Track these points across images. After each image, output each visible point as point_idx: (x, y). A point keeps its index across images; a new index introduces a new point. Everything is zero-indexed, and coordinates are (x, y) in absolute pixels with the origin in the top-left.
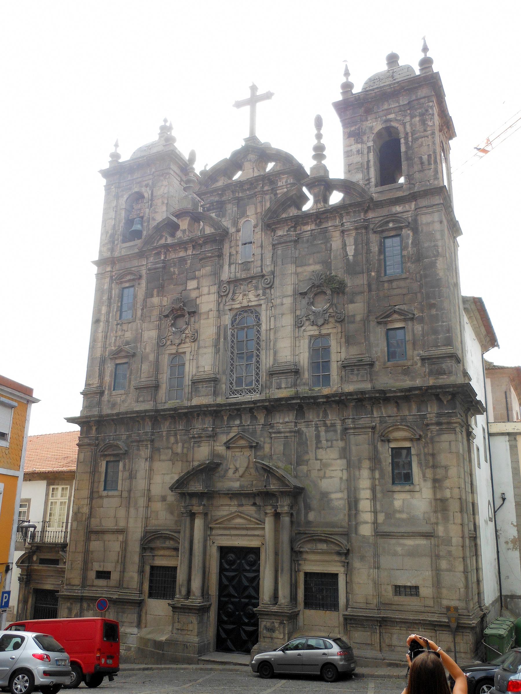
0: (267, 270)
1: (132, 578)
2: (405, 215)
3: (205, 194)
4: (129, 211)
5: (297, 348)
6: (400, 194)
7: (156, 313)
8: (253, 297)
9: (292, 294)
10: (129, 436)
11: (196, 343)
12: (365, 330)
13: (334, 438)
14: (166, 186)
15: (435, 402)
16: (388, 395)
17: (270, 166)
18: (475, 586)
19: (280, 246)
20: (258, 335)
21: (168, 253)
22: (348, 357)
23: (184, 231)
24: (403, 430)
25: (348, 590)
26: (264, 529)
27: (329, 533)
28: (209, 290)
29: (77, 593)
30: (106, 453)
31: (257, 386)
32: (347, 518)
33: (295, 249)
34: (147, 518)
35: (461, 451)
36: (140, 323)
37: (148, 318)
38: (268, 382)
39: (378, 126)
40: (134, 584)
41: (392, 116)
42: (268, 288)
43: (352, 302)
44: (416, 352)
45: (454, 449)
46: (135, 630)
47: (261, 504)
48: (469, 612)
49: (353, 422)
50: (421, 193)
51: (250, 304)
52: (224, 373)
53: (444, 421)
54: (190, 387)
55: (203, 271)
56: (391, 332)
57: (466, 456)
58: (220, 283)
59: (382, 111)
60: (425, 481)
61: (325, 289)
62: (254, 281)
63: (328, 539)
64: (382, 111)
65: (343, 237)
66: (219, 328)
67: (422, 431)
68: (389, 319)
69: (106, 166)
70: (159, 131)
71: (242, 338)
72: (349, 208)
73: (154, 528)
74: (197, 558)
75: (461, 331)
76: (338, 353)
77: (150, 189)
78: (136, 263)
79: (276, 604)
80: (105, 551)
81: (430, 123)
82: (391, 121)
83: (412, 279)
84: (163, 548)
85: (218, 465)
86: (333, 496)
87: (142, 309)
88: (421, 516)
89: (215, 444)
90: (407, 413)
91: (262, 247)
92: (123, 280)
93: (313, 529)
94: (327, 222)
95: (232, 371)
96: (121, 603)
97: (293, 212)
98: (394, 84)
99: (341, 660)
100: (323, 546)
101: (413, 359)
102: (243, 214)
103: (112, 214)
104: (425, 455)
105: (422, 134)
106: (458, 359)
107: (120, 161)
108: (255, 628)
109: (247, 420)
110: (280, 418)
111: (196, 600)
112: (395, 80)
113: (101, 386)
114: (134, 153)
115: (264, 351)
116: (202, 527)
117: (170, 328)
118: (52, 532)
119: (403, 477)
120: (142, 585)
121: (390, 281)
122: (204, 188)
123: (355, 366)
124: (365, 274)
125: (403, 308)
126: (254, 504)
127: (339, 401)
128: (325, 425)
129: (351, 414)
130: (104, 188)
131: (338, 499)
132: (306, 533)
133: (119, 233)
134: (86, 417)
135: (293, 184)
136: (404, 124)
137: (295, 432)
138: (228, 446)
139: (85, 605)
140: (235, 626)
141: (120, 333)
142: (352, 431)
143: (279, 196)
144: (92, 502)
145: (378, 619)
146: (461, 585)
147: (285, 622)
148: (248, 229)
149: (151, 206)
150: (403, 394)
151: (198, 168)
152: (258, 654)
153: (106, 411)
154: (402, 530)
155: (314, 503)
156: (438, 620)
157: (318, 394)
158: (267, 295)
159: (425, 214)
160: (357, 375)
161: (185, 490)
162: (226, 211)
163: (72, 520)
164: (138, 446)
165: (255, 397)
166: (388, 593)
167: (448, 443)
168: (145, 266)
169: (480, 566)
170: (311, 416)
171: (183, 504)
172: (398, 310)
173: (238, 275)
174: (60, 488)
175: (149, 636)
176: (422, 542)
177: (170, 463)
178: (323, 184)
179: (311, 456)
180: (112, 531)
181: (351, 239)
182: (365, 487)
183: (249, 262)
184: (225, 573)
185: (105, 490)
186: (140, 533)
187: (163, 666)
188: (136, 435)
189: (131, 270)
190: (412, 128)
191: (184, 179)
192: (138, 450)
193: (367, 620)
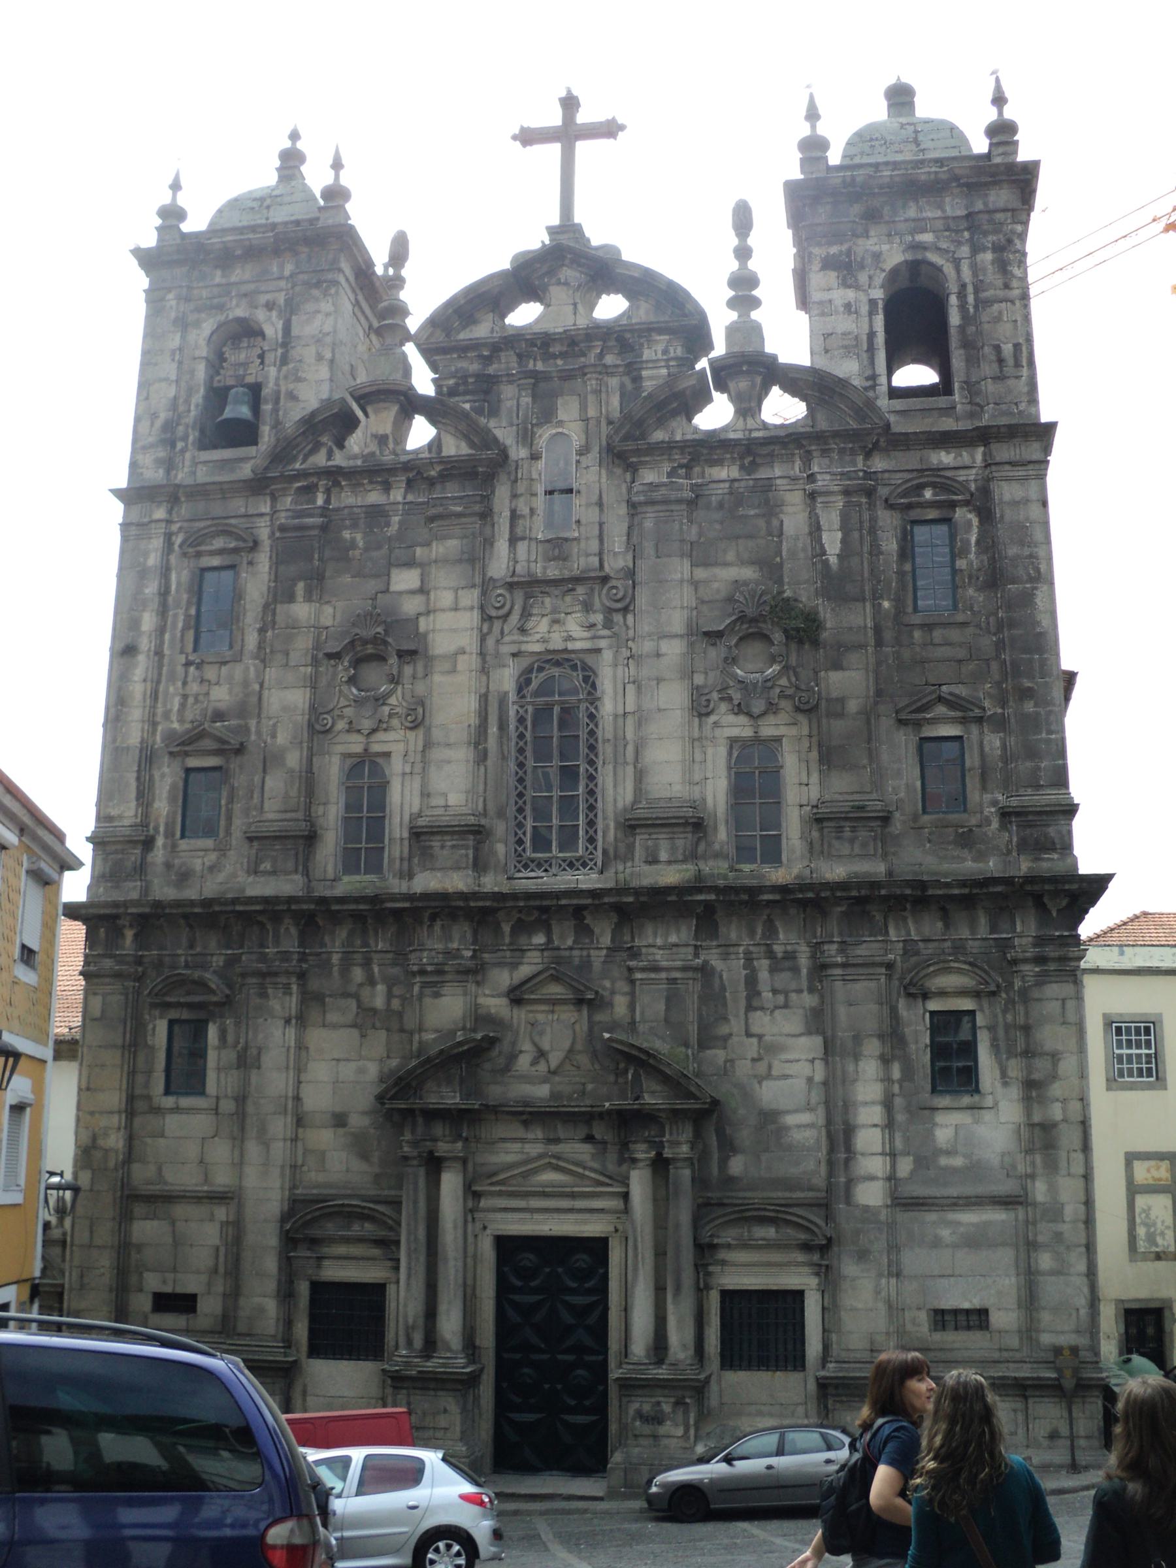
0: (616, 563)
1: (261, 1310)
2: (962, 476)
4: (217, 362)
5: (697, 767)
7: (303, 644)
8: (578, 628)
10: (231, 961)
11: (421, 732)
13: (793, 986)
14: (328, 315)
19: (649, 509)
21: (335, 491)
22: (827, 797)
24: (959, 971)
27: (783, 1202)
28: (456, 598)
30: (168, 999)
31: (591, 853)
32: (823, 1169)
34: (294, 1167)
36: (254, 665)
37: (279, 657)
39: (894, 256)
41: (927, 237)
43: (837, 666)
44: (987, 797)
52: (501, 814)
53: (1052, 955)
54: (406, 843)
55: (438, 549)
58: (486, 586)
59: (906, 220)
60: (1005, 1084)
61: (766, 627)
62: (581, 590)
63: (780, 1215)
66: (484, 698)
71: (552, 728)
73: (315, 1191)
74: (451, 1263)
76: (800, 785)
77: (279, 317)
78: (238, 505)
82: (925, 249)
83: (978, 626)
84: (347, 1240)
85: (491, 1042)
86: (790, 1120)
87: (262, 631)
88: (995, 1161)
90: (965, 933)
92: (203, 548)
93: (741, 1194)
94: (771, 465)
100: (770, 1232)
101: (982, 812)
102: (547, 415)
104: (1007, 1027)
105: (1001, 293)
107: (185, 227)
110: (655, 935)
113: (144, 825)
115: (611, 767)
117: (345, 688)
119: (953, 1068)
121: (928, 627)
124: (868, 604)
125: (957, 692)
126: (589, 1139)
127: (808, 901)
128: (770, 954)
129: (836, 932)
130: (143, 295)
131: (803, 1126)
136: (957, 263)
141: (194, 688)
142: (838, 971)
144: (131, 1124)
146: (1082, 1301)
153: (162, 890)
154: (953, 1191)
155: (744, 1136)
156: (1035, 1375)
159: (1008, 479)
160: (852, 841)
162: (499, 401)
164: (262, 986)
165: (587, 880)
167: (1060, 1002)
170: (732, 931)
173: (538, 570)
176: (997, 1216)
177: (355, 1033)
179: (735, 1025)
181: (834, 514)
183: (566, 540)
188: (254, 957)
192: (264, 995)
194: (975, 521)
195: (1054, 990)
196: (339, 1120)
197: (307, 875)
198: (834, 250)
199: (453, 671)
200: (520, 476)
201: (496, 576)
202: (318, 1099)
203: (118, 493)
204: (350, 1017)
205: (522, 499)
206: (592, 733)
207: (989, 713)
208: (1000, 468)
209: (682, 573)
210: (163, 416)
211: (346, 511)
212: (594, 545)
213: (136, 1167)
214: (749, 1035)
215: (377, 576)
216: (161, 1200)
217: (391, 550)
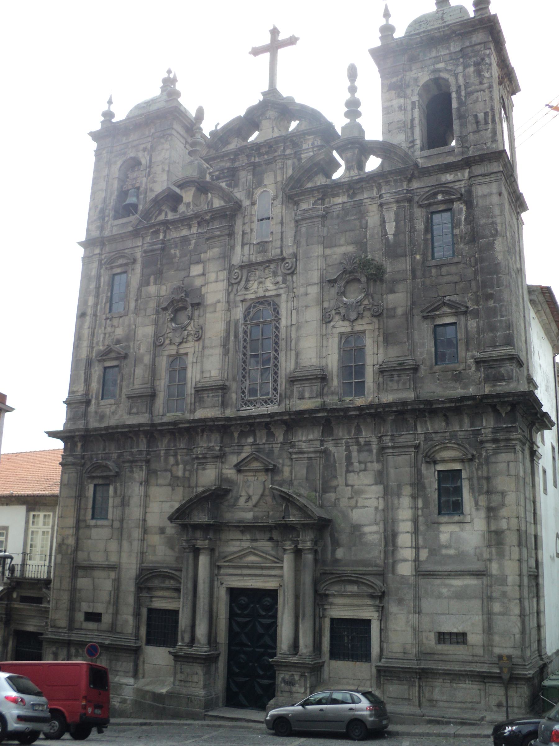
0: (288, 252)
1: (126, 621)
2: (457, 185)
3: (214, 159)
4: (123, 180)
5: (324, 349)
6: (451, 159)
7: (152, 305)
8: (271, 285)
9: (319, 281)
10: (120, 456)
11: (201, 342)
12: (408, 326)
14: (167, 150)
16: (434, 406)
17: (294, 125)
18: (534, 632)
19: (304, 222)
20: (277, 332)
22: (386, 360)
23: (188, 205)
24: (453, 448)
25: (383, 639)
26: (282, 568)
29: (64, 636)
30: (94, 474)
31: (275, 396)
33: (323, 226)
34: (142, 553)
35: (521, 474)
38: (288, 391)
39: (424, 77)
40: (129, 628)
41: (441, 65)
42: (289, 274)
43: (392, 291)
44: (469, 354)
45: (513, 472)
46: (131, 681)
47: (279, 539)
48: (524, 661)
49: (392, 440)
50: (477, 158)
51: (267, 294)
52: (234, 379)
54: (193, 396)
55: (211, 253)
56: (439, 329)
57: (529, 479)
58: (231, 268)
59: (430, 59)
60: (477, 509)
61: (358, 275)
62: (272, 266)
63: (359, 580)
64: (430, 59)
65: (382, 211)
66: (228, 323)
67: (476, 450)
68: (437, 313)
69: (97, 127)
70: (162, 84)
71: (257, 337)
72: (389, 177)
73: (151, 565)
74: (202, 600)
75: (525, 328)
76: (374, 355)
79: (296, 654)
80: (94, 589)
81: (487, 75)
82: (440, 71)
83: (465, 263)
84: (163, 589)
85: (227, 491)
86: (367, 529)
87: (137, 300)
90: (457, 428)
91: (282, 223)
94: (362, 192)
95: (244, 377)
96: (114, 650)
97: (320, 180)
98: (444, 27)
99: (371, 716)
100: (354, 588)
101: (466, 363)
102: (260, 183)
103: (103, 185)
104: (479, 478)
105: (478, 87)
106: (519, 362)
107: (114, 120)
108: (272, 681)
109: (262, 438)
110: (302, 435)
111: (202, 648)
112: (445, 22)
113: (87, 394)
114: (131, 111)
115: (284, 352)
116: (208, 566)
117: (169, 324)
118: (34, 566)
120: (138, 631)
121: (439, 266)
122: (212, 152)
123: (395, 370)
124: (408, 258)
126: (271, 539)
127: (375, 414)
128: (358, 443)
130: (94, 153)
131: (373, 532)
132: (332, 574)
133: (110, 207)
134: (70, 431)
135: (321, 147)
136: (456, 76)
137: (320, 452)
139: (73, 651)
140: (248, 679)
141: (109, 329)
142: (391, 451)
143: (303, 161)
144: (78, 531)
145: (417, 671)
146: (517, 630)
147: (306, 674)
148: (265, 201)
149: (149, 175)
150: (453, 405)
151: (207, 128)
152: (274, 708)
153: (94, 424)
155: (344, 538)
156: (488, 671)
157: (350, 406)
158: (288, 283)
159: (480, 184)
160: (398, 382)
161: (186, 521)
163: (55, 553)
164: (131, 467)
165: (272, 408)
166: (430, 641)
168: (140, 248)
169: (542, 609)
171: (185, 538)
173: (253, 258)
174: (42, 514)
175: (148, 688)
176: (472, 582)
177: (170, 488)
178: (358, 148)
179: (340, 481)
180: (101, 567)
182: (405, 518)
183: (266, 242)
184: (236, 619)
185: (93, 518)
186: (134, 571)
187: (163, 721)
188: (128, 453)
189: (124, 253)
190: (465, 80)
191: (190, 140)
192: (132, 471)
194: (464, 208)
197: (152, 414)
199: (215, 311)
203: (81, 244)
204: (168, 481)
205: (247, 225)
208: (476, 178)
209: (318, 252)
210: (100, 207)
212: (278, 243)
213: (80, 553)
214: (347, 485)
215: (184, 270)
216: (90, 568)
217: (191, 256)
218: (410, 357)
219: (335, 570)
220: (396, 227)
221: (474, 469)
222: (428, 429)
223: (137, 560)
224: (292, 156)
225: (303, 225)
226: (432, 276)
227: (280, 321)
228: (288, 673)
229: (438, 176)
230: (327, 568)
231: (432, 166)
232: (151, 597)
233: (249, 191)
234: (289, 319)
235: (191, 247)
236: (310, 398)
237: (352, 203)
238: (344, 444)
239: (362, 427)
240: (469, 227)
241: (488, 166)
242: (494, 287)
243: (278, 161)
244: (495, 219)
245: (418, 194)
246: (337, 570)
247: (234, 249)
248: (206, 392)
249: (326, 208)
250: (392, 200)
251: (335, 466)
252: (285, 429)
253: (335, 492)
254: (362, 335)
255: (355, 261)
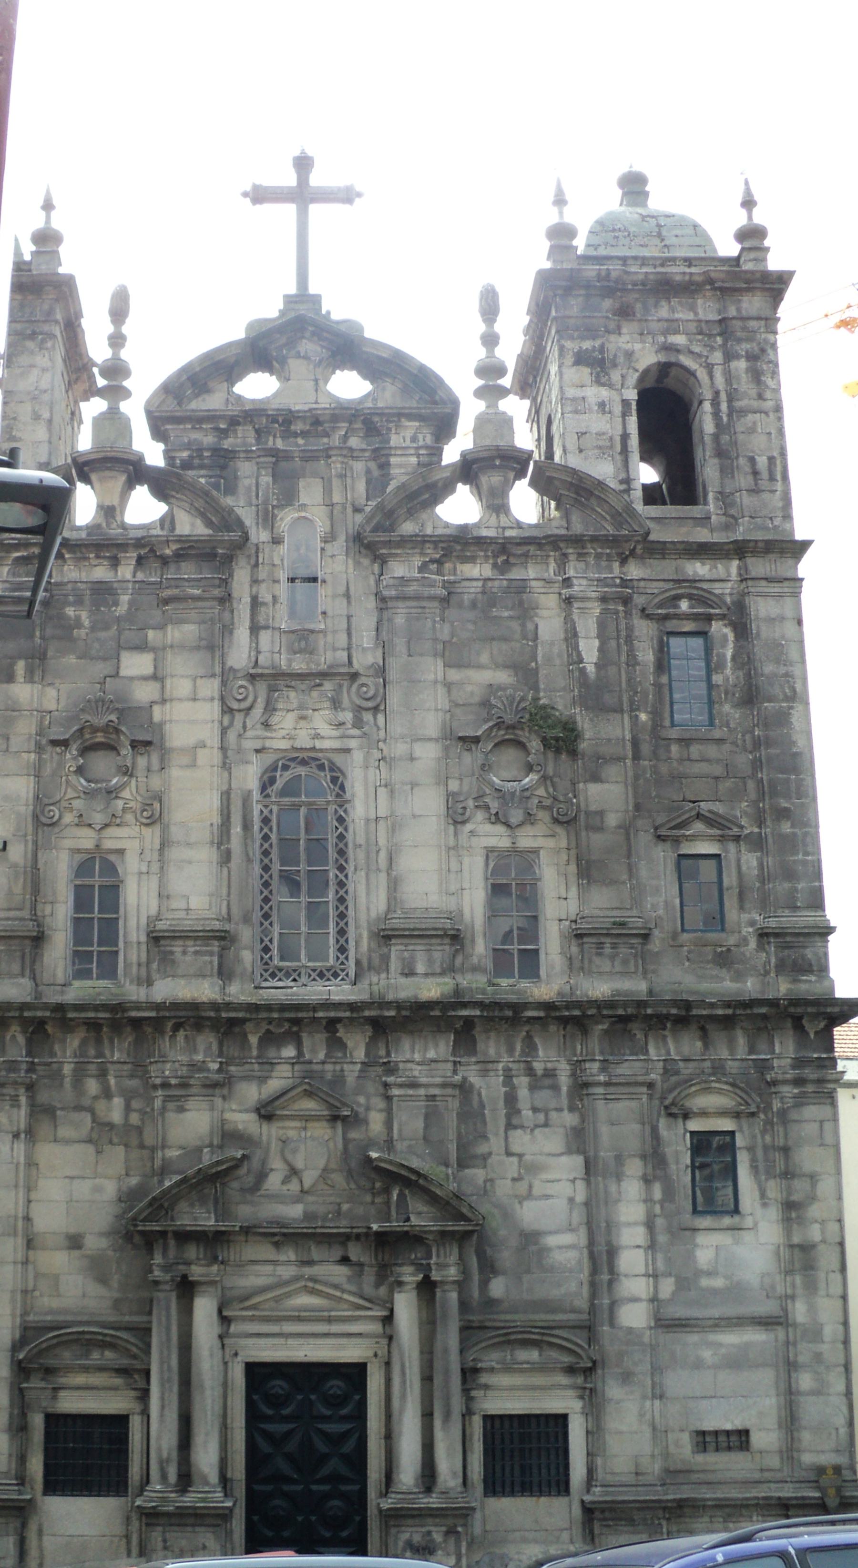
0: (366, 659)
2: (717, 589)
7: (24, 729)
8: (326, 726)
11: (157, 829)
13: (553, 1104)
14: (44, 370)
15: (791, 1032)
16: (694, 1012)
19: (400, 604)
24: (720, 1092)
32: (585, 1291)
39: (648, 357)
41: (680, 340)
43: (596, 778)
44: (745, 917)
49: (603, 1070)
51: (319, 744)
52: (246, 919)
55: (174, 634)
58: (226, 676)
59: (659, 320)
60: (765, 1205)
61: (523, 735)
62: (328, 686)
64: (659, 320)
66: (226, 796)
67: (760, 1095)
71: (296, 839)
72: (589, 546)
73: (49, 1318)
74: (208, 1393)
76: (559, 900)
82: (678, 351)
83: (734, 743)
86: (552, 1241)
89: (226, 1106)
90: (724, 1054)
93: (503, 1317)
95: (266, 916)
100: (533, 1355)
101: (740, 932)
102: (289, 497)
104: (766, 1148)
105: (755, 404)
109: (315, 1047)
115: (363, 873)
117: (73, 778)
126: (345, 1260)
127: (570, 1018)
128: (530, 1072)
129: (597, 1051)
131: (565, 1247)
136: (710, 368)
138: (266, 1112)
142: (600, 1090)
146: (840, 1421)
147: (460, 1529)
154: (716, 1313)
155: (506, 1257)
156: (794, 1495)
159: (765, 596)
160: (612, 958)
165: (340, 991)
166: (683, 1448)
170: (490, 1046)
172: (707, 814)
176: (756, 1336)
177: (91, 1149)
179: (495, 1144)
181: (590, 621)
182: (631, 1219)
183: (312, 631)
193: (638, 1509)
194: (731, 636)
195: (811, 1111)
196: (75, 1242)
197: (34, 979)
198: (587, 345)
199: (193, 765)
200: (261, 560)
201: (236, 667)
202: (50, 1219)
205: (263, 586)
206: (341, 837)
207: (747, 832)
208: (757, 583)
209: (436, 674)
211: (70, 586)
214: (509, 1154)
215: (105, 659)
217: (120, 632)
218: (635, 912)
219: (490, 1320)
220: (601, 650)
221: (757, 1131)
222: (669, 1053)
223: (14, 1309)
224: (367, 454)
225: (399, 611)
226: (670, 758)
227: (347, 806)
228: (419, 1529)
229: (679, 561)
230: (471, 1318)
231: (673, 543)
232: (56, 1390)
233: (266, 511)
234: (373, 805)
235: (122, 609)
236: (426, 975)
237: (505, 583)
238: (501, 1072)
239: (537, 1040)
240: (741, 674)
241: (778, 564)
242: (791, 798)
243: (334, 459)
244: (791, 669)
245: (641, 590)
246: (495, 1320)
247: (231, 632)
248: (180, 942)
249: (449, 582)
250: (594, 595)
251: (484, 1115)
252: (369, 1034)
253: (485, 1167)
254: (533, 856)
255: (523, 705)
